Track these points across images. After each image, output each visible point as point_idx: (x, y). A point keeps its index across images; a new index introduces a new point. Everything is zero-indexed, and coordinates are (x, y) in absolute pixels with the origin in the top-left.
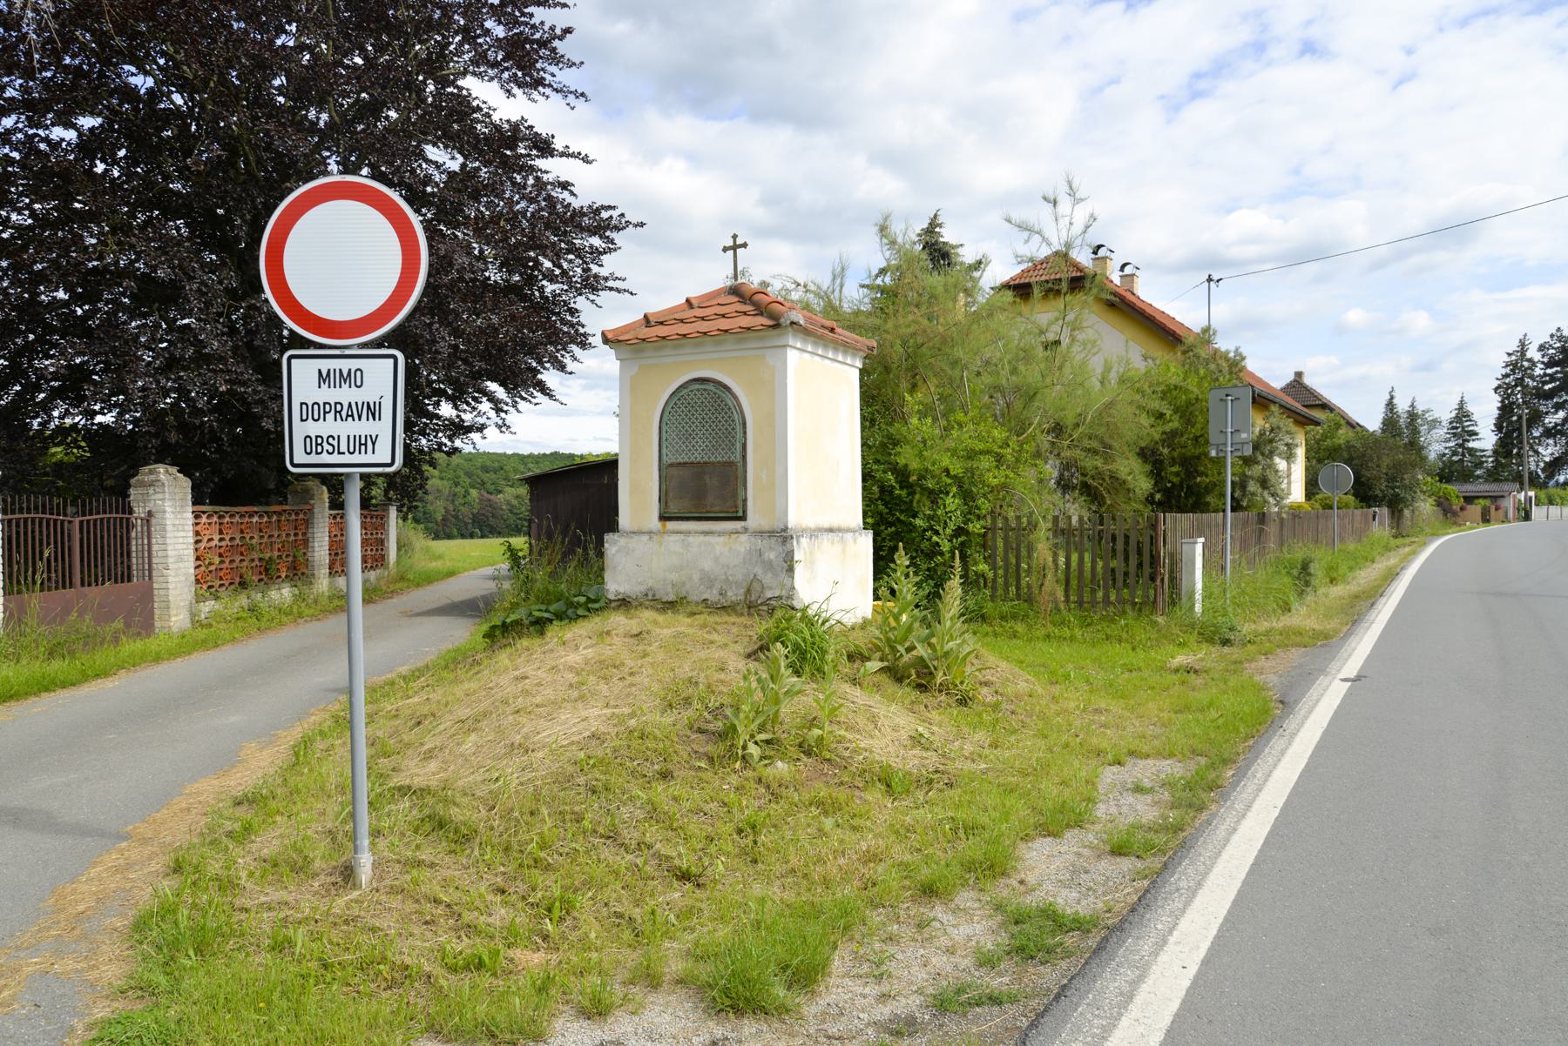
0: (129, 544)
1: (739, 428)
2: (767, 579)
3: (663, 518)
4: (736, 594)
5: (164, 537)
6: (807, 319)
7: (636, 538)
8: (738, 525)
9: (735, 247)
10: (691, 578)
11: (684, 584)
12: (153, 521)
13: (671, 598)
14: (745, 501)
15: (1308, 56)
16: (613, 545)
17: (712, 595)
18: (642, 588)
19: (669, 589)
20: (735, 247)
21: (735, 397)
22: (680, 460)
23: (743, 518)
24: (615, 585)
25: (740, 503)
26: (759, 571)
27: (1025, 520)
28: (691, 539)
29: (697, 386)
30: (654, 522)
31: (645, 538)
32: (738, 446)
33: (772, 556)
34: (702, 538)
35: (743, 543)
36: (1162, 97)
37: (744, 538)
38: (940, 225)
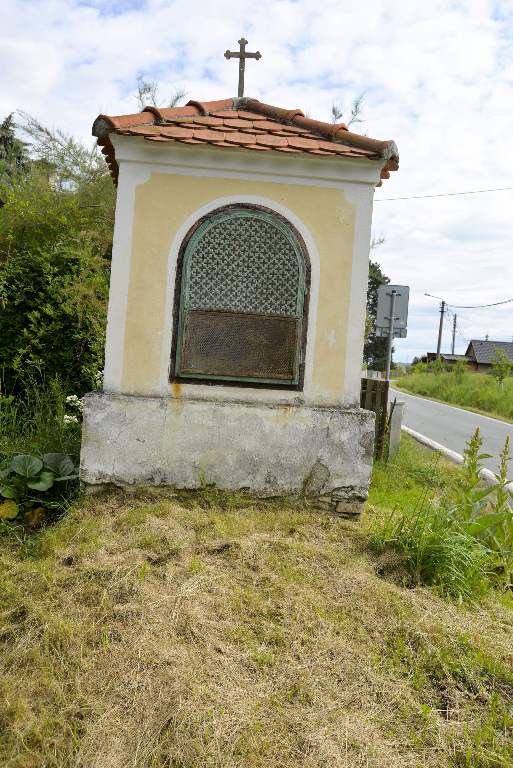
1: (302, 276)
2: (336, 465)
3: (176, 378)
4: (287, 483)
7: (138, 403)
8: (290, 396)
10: (223, 460)
11: (212, 467)
13: (192, 483)
14: (302, 366)
15: (207, 79)
16: (96, 413)
17: (256, 483)
18: (146, 471)
19: (189, 472)
20: (243, 56)
21: (299, 236)
22: (210, 305)
23: (299, 388)
24: (95, 464)
25: (296, 369)
26: (325, 454)
28: (227, 410)
29: (245, 214)
30: (162, 383)
31: (154, 405)
32: (300, 297)
33: (344, 437)
34: (243, 409)
35: (304, 420)
36: (117, 81)
37: (306, 413)
38: (13, 125)
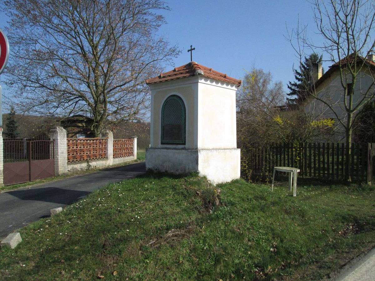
0: (49, 148)
1: (183, 113)
3: (162, 143)
5: (57, 147)
6: (205, 72)
9: (191, 50)
12: (55, 142)
20: (191, 50)
23: (184, 144)
27: (313, 144)
32: (183, 118)
